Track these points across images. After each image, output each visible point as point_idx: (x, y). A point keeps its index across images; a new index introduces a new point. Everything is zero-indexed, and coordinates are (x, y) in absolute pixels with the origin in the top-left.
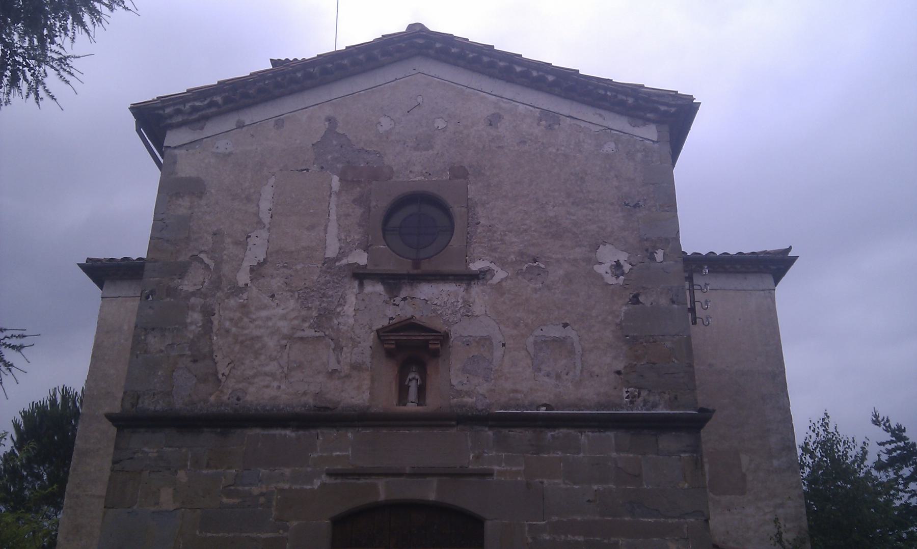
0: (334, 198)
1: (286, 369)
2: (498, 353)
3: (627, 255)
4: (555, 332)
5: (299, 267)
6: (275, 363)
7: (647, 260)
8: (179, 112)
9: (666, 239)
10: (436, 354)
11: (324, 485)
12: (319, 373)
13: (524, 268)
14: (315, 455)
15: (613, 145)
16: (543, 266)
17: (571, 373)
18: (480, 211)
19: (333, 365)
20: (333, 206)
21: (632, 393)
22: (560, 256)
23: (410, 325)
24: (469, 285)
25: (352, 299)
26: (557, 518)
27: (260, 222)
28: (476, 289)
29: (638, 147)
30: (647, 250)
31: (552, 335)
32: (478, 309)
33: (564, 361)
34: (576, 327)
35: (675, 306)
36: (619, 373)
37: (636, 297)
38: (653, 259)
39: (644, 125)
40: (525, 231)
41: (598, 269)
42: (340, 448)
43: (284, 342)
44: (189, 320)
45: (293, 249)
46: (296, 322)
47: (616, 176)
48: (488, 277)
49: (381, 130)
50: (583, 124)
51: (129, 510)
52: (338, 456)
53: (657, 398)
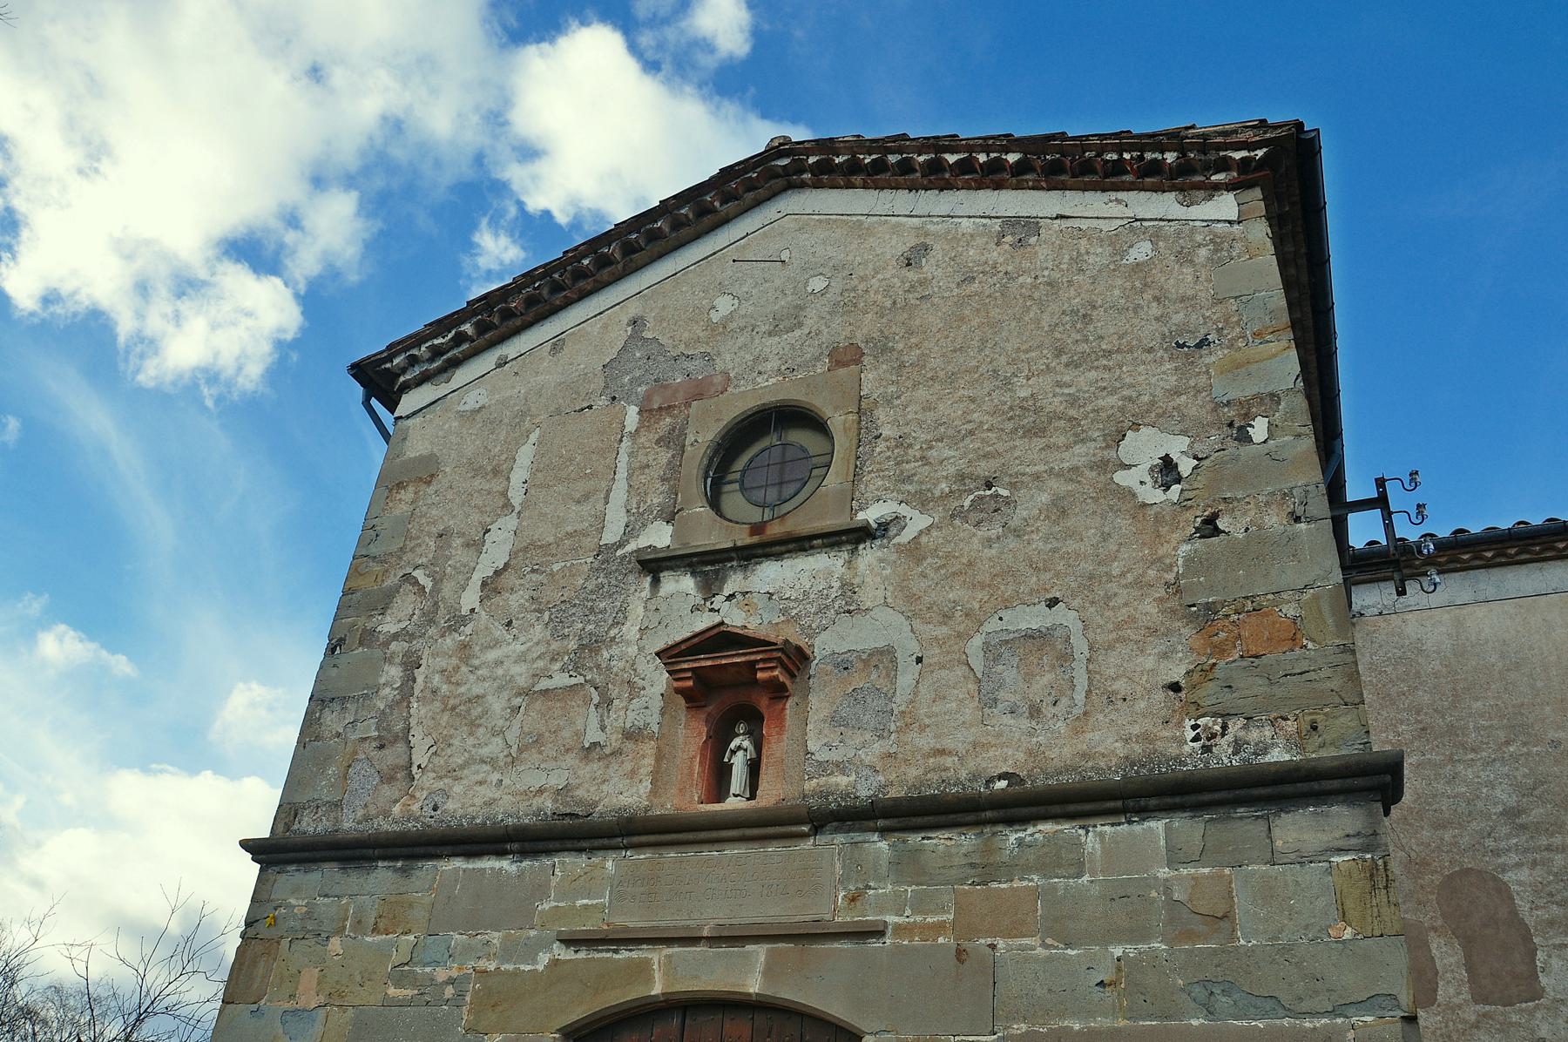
0: (626, 443)
1: (514, 751)
2: (907, 677)
3: (1187, 440)
4: (1034, 618)
5: (556, 567)
6: (499, 740)
7: (1231, 444)
8: (413, 361)
9: (1272, 395)
10: (778, 692)
11: (555, 963)
12: (567, 751)
13: (967, 503)
14: (546, 906)
15: (1148, 245)
16: (1005, 493)
17: (1064, 701)
18: (881, 414)
19: (594, 735)
20: (623, 459)
21: (1206, 728)
22: (1041, 468)
23: (720, 639)
24: (854, 551)
25: (637, 610)
26: (1024, 1027)
27: (507, 506)
28: (869, 555)
29: (1199, 238)
30: (1231, 425)
31: (1023, 626)
32: (868, 596)
33: (1048, 678)
34: (1076, 603)
35: (1303, 526)
36: (1175, 687)
37: (1210, 521)
38: (1244, 437)
39: (1210, 197)
40: (971, 433)
41: (1121, 478)
42: (588, 886)
43: (517, 701)
44: (382, 680)
45: (551, 539)
46: (540, 664)
47: (1157, 299)
48: (893, 531)
49: (715, 317)
50: (1084, 225)
51: (254, 1007)
52: (586, 907)
53: (1268, 732)
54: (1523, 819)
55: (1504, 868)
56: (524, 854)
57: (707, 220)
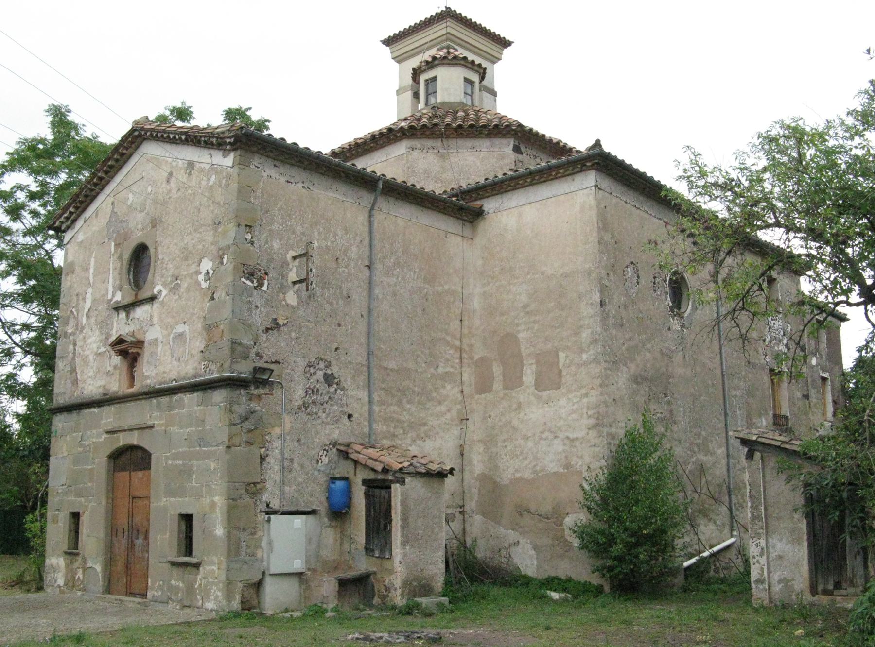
42: (108, 417)
54: (528, 309)
55: (519, 332)
56: (99, 406)
57: (125, 157)
